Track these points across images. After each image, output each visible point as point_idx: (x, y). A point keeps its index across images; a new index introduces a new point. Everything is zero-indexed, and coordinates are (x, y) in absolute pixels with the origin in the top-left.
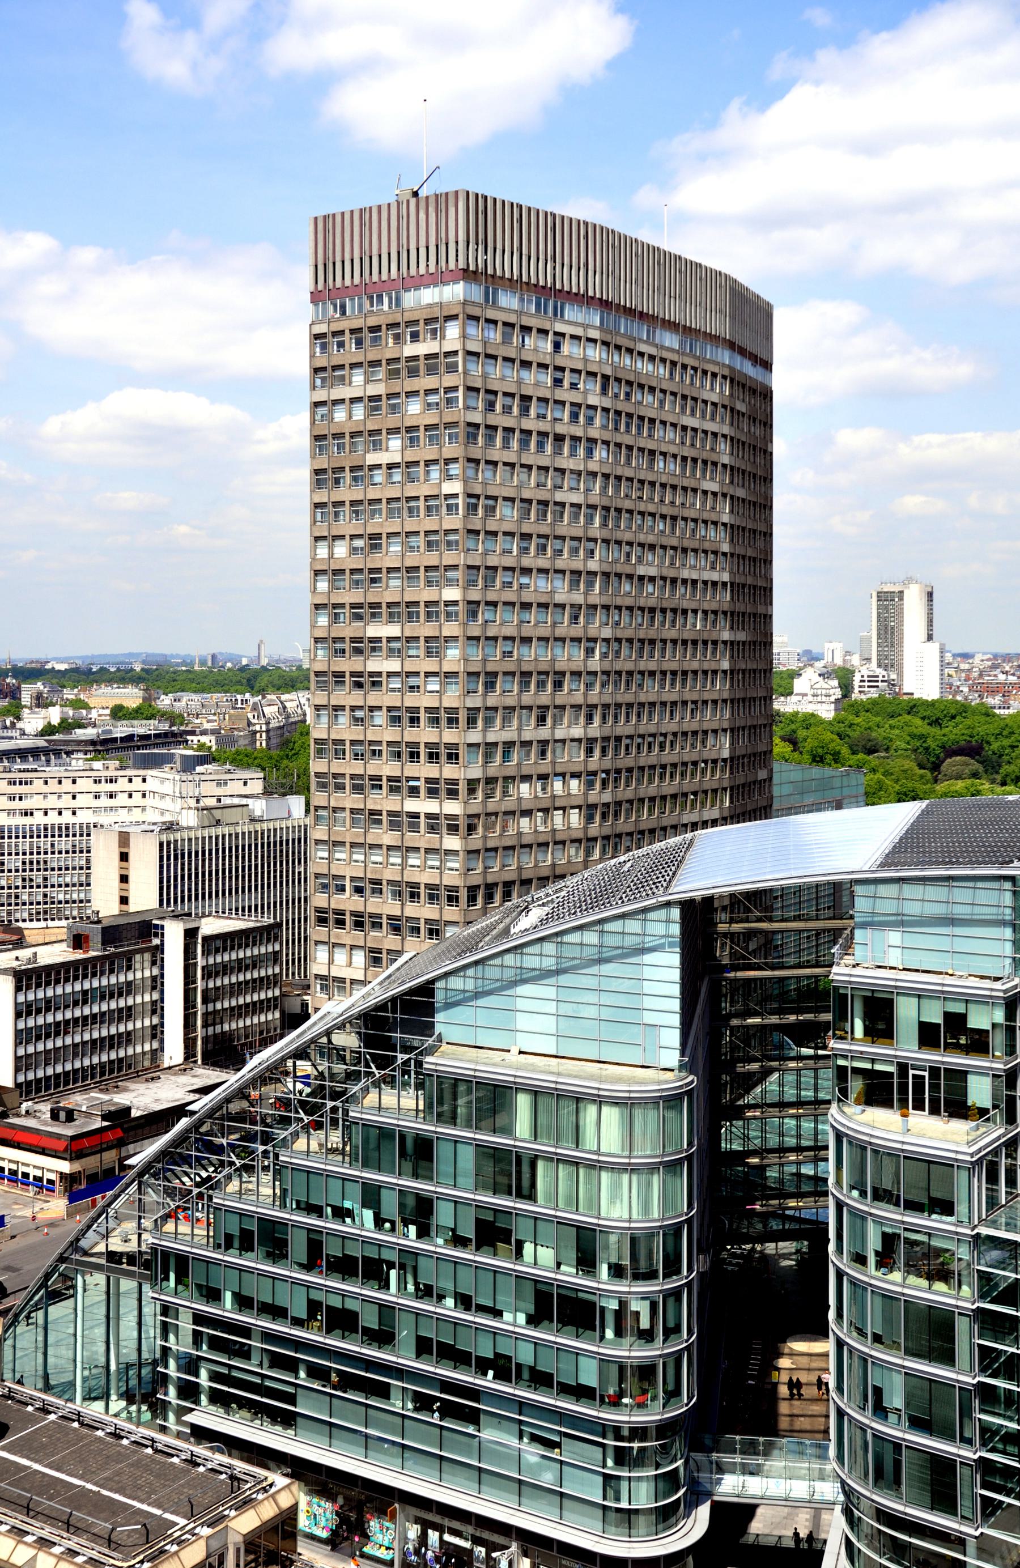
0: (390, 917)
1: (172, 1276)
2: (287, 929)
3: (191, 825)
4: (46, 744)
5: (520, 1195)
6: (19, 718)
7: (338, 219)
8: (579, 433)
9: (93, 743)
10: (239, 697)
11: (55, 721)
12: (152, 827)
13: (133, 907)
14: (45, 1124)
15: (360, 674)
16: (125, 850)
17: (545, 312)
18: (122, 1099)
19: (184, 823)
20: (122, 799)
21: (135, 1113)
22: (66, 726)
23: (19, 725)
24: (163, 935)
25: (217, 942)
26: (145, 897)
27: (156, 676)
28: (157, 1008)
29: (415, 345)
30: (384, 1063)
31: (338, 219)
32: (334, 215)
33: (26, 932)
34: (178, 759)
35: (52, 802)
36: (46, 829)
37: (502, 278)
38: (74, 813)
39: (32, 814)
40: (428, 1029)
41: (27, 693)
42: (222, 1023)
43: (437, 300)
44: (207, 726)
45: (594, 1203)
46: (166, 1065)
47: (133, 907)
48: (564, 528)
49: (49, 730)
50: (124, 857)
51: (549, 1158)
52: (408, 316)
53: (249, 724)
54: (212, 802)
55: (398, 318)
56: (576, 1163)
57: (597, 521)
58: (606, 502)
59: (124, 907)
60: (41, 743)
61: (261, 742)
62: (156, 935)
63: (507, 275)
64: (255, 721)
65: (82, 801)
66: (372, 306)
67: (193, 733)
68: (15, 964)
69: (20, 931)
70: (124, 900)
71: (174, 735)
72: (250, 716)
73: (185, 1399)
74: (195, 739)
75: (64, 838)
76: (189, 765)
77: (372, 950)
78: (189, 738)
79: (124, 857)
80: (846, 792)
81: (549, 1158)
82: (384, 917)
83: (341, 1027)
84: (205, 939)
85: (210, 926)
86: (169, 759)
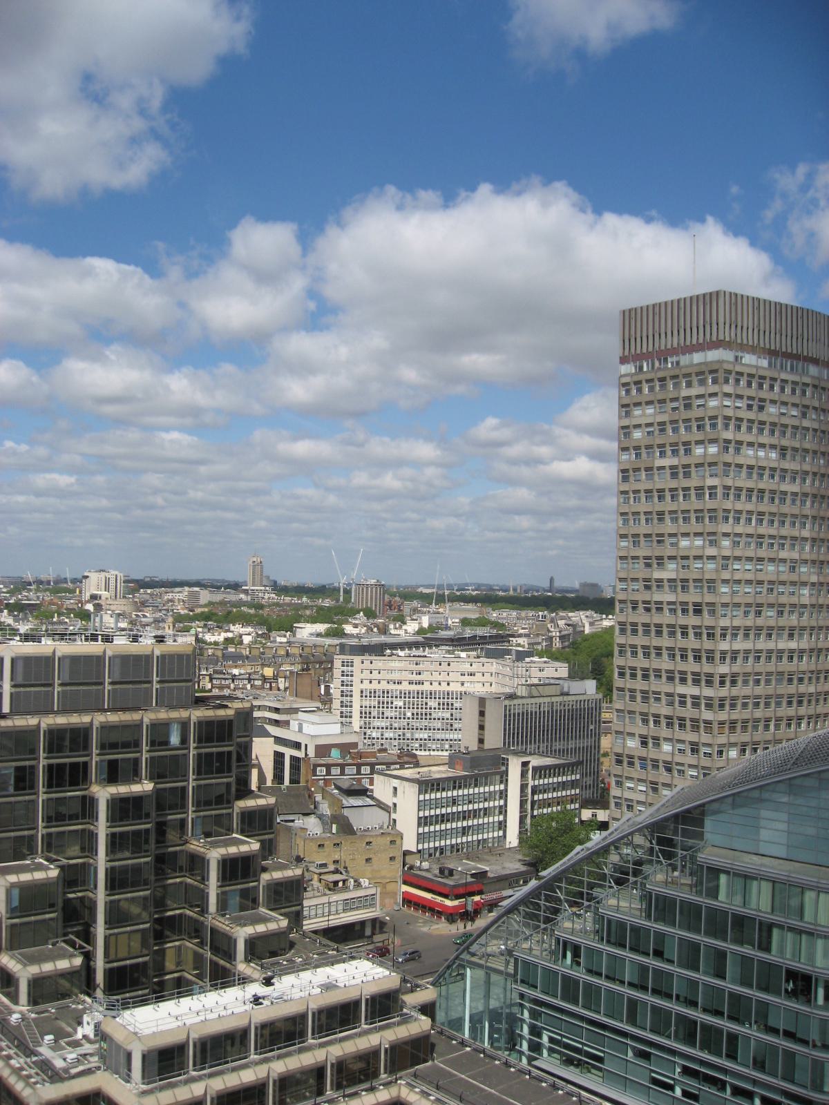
0: (665, 762)
1: (569, 955)
2: (586, 765)
3: (524, 695)
4: (232, 628)
5: (760, 948)
6: (405, 623)
7: (639, 311)
8: (797, 445)
9: (452, 640)
10: (540, 613)
11: (426, 625)
12: (499, 696)
13: (488, 745)
14: (436, 876)
15: (648, 602)
16: (482, 709)
17: (786, 369)
18: (484, 867)
19: (519, 694)
20: (478, 677)
21: (490, 875)
22: (432, 628)
23: (404, 627)
24: (508, 764)
25: (540, 771)
26: (494, 739)
27: (489, 599)
28: (503, 810)
29: (689, 389)
30: (669, 856)
31: (639, 311)
32: (636, 309)
33: (419, 757)
34: (513, 652)
35: (436, 676)
36: (431, 694)
37: (747, 345)
38: (448, 684)
39: (423, 684)
40: (700, 836)
41: (407, 607)
42: (483, 833)
43: (703, 361)
44: (521, 631)
45: (811, 958)
46: (507, 847)
47: (487, 746)
48: (786, 509)
49: (421, 631)
50: (482, 714)
51: (781, 927)
52: (684, 371)
53: (549, 631)
54: (536, 681)
55: (677, 372)
56: (799, 932)
57: (808, 503)
58: (815, 491)
59: (481, 745)
60: (420, 638)
61: (557, 644)
62: (503, 764)
63: (751, 343)
64: (552, 630)
65: (452, 677)
66: (660, 364)
67: (513, 636)
68: (418, 776)
69: (415, 756)
70: (481, 741)
71: (502, 637)
72: (549, 626)
73: (533, 1052)
74: (514, 640)
75: (373, 698)
76: (520, 656)
77: (652, 783)
78: (511, 639)
79: (482, 714)
80: (256, 703)
81: (781, 927)
82: (661, 761)
83: (639, 830)
84: (535, 769)
85: (535, 761)
86: (508, 652)
